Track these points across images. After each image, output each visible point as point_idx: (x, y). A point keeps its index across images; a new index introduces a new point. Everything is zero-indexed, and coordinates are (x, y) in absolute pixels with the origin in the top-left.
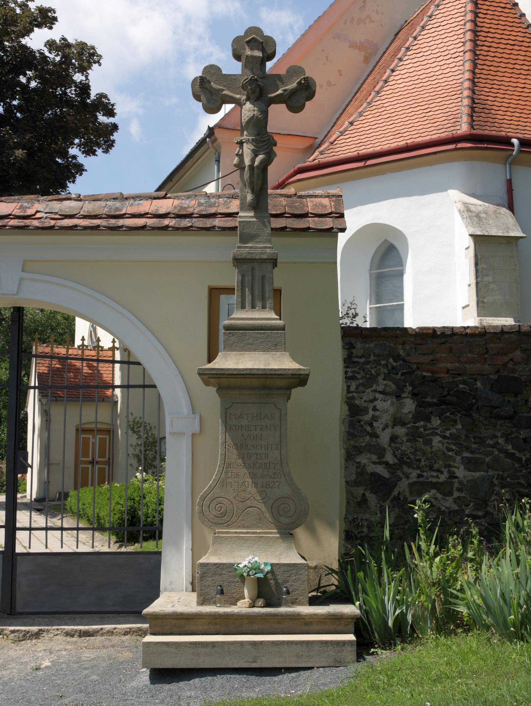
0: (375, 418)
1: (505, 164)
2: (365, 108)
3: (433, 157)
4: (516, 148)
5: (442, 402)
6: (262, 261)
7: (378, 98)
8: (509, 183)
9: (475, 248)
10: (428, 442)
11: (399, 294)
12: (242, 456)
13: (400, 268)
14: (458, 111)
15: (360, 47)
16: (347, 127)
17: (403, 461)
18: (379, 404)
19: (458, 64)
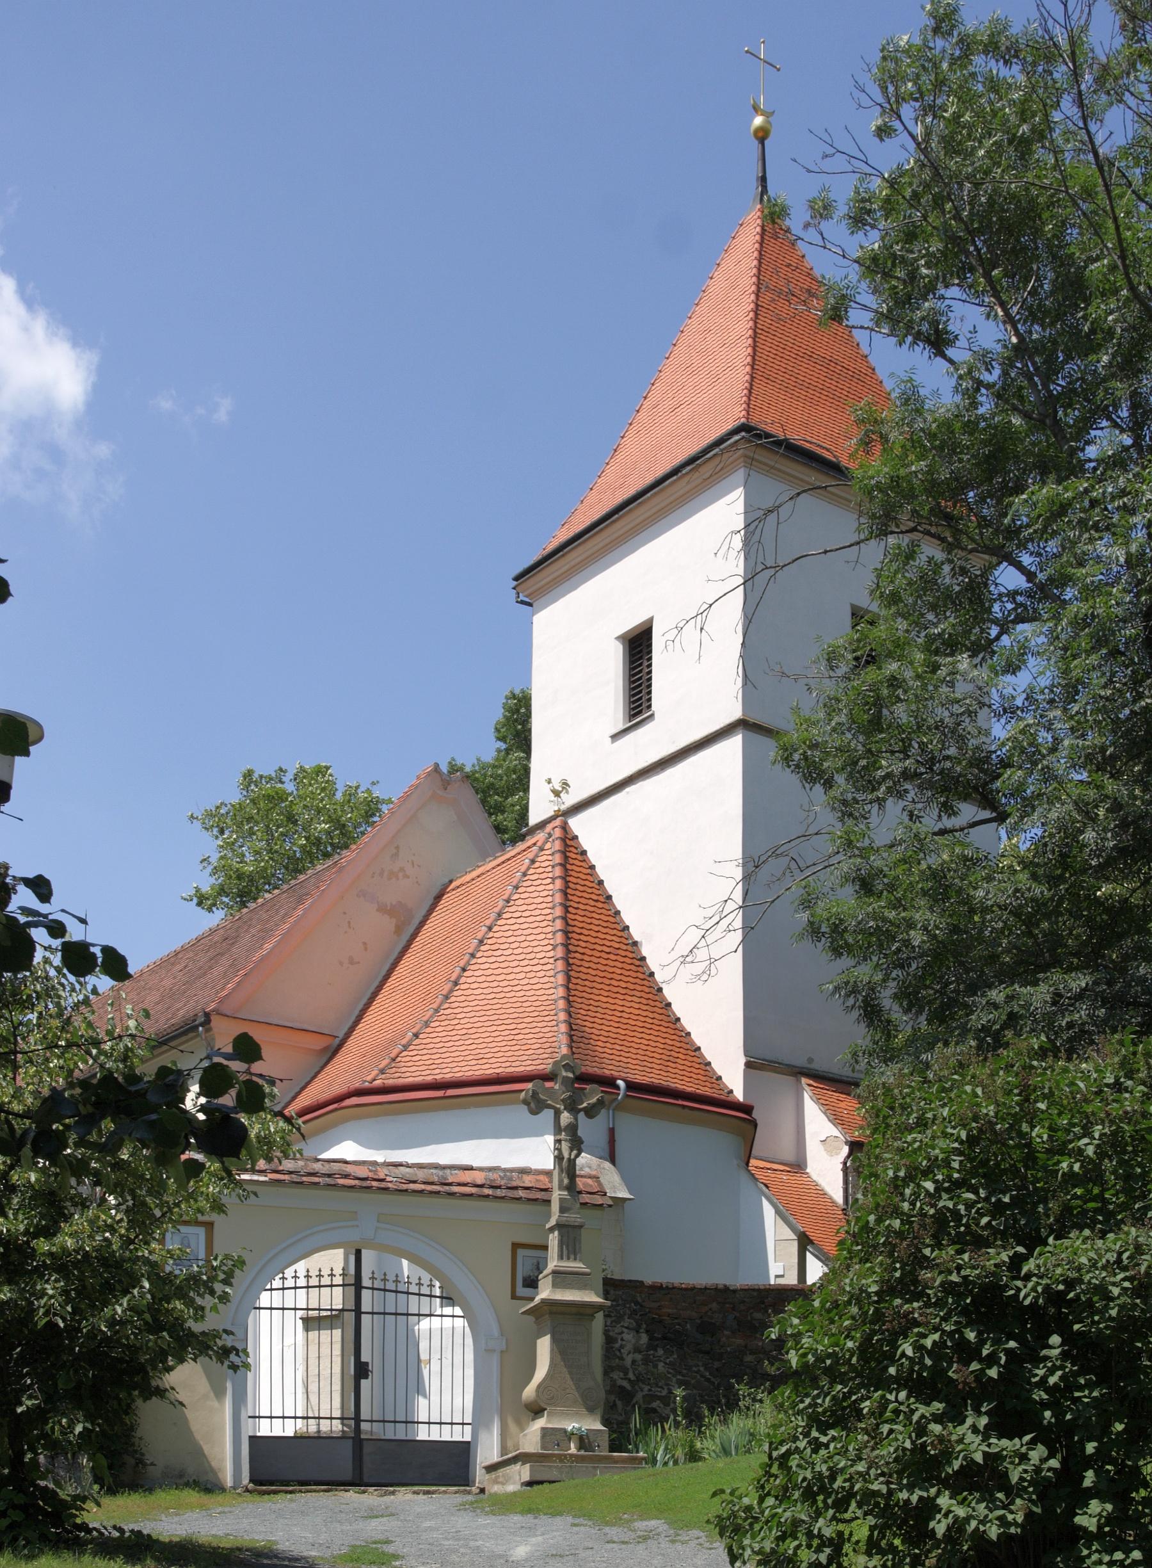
0: (622, 1346)
4: (622, 1092)
5: (664, 1338)
6: (575, 1227)
7: (447, 1005)
8: (612, 1131)
10: (656, 1366)
12: (563, 1360)
14: (554, 1039)
16: (411, 1040)
17: (639, 1379)
18: (625, 1336)
19: (548, 974)
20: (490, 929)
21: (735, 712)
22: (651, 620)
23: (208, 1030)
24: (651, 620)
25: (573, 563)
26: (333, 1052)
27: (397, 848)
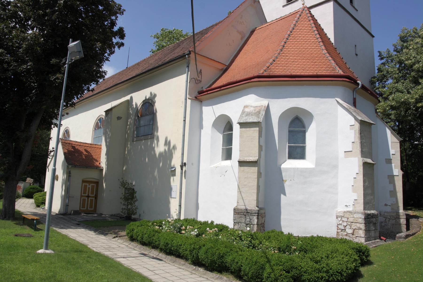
20: (291, 32)
23: (189, 57)
26: (225, 71)
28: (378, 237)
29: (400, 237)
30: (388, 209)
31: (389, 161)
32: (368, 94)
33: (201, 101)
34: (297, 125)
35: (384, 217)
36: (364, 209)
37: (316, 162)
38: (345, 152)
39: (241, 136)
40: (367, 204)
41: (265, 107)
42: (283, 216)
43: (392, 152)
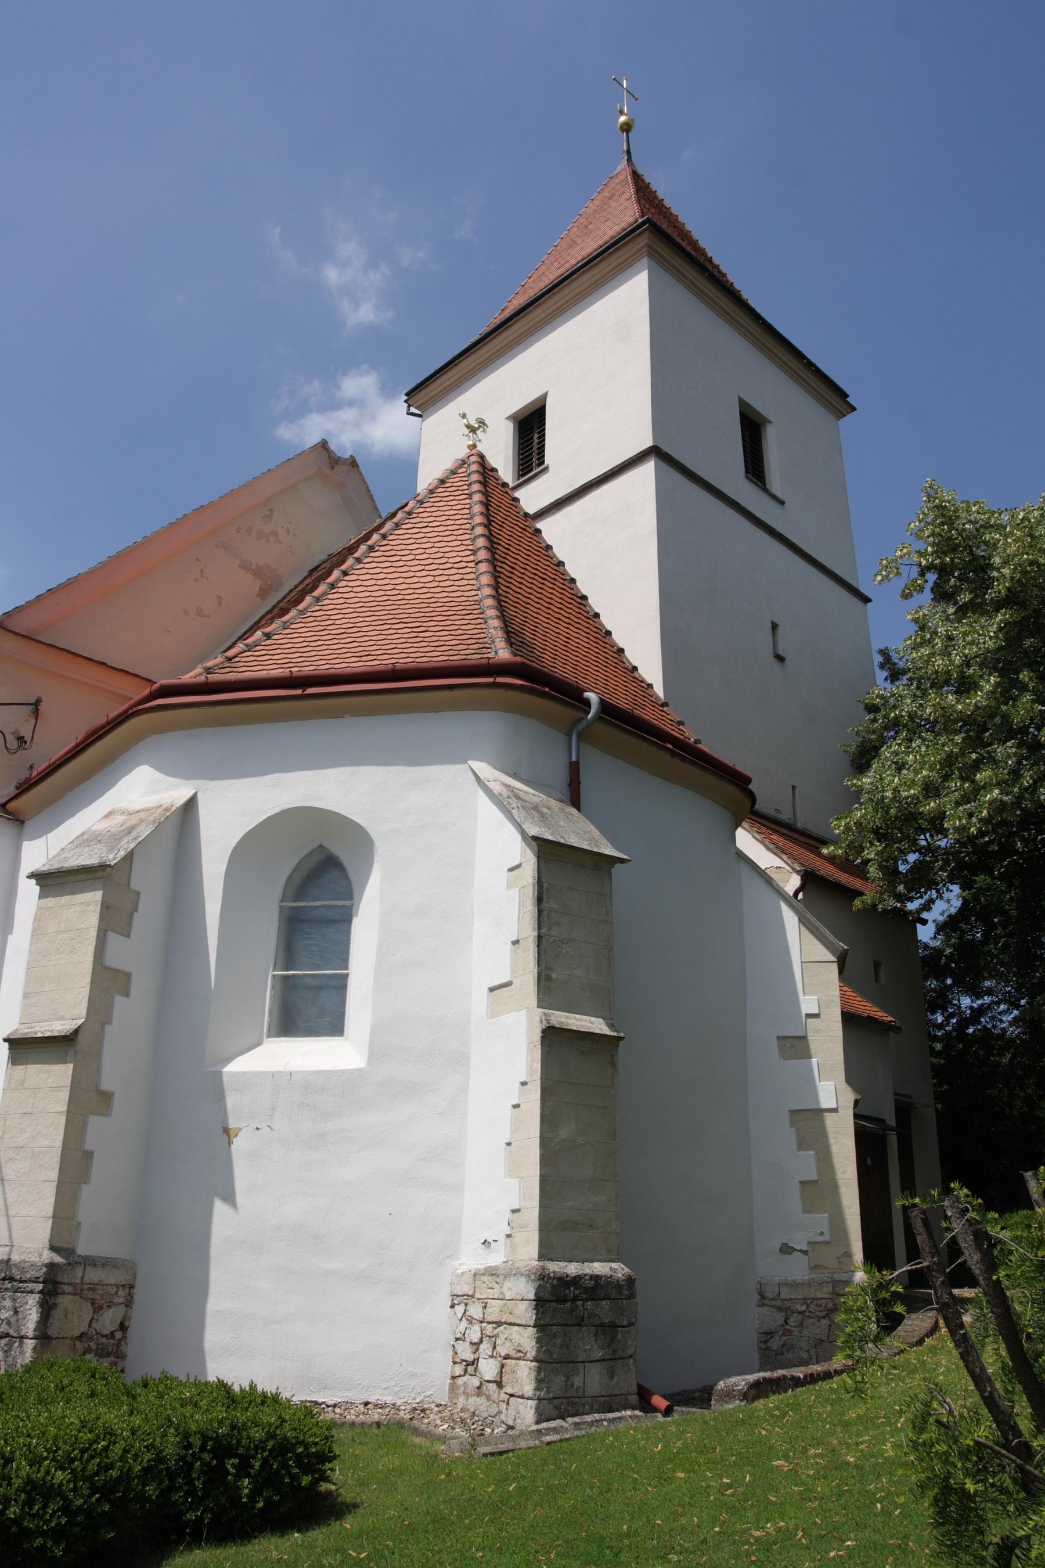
1: (569, 736)
2: (292, 618)
3: (447, 694)
9: (538, 866)
11: (340, 953)
13: (347, 903)
15: (257, 572)
21: (648, 443)
22: (543, 398)
24: (543, 398)
25: (465, 371)
27: (271, 511)
28: (634, 1399)
29: (728, 1395)
30: (798, 1269)
31: (796, 1046)
32: (666, 756)
33: (22, 822)
34: (314, 883)
35: (780, 1309)
36: (545, 1253)
37: (372, 1043)
38: (491, 990)
39: (37, 932)
40: (557, 1229)
41: (167, 810)
42: (219, 1302)
43: (808, 1004)
